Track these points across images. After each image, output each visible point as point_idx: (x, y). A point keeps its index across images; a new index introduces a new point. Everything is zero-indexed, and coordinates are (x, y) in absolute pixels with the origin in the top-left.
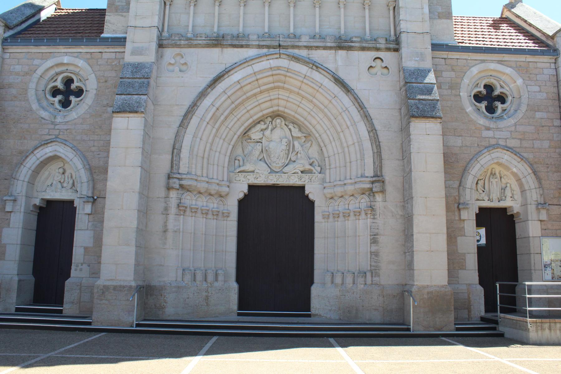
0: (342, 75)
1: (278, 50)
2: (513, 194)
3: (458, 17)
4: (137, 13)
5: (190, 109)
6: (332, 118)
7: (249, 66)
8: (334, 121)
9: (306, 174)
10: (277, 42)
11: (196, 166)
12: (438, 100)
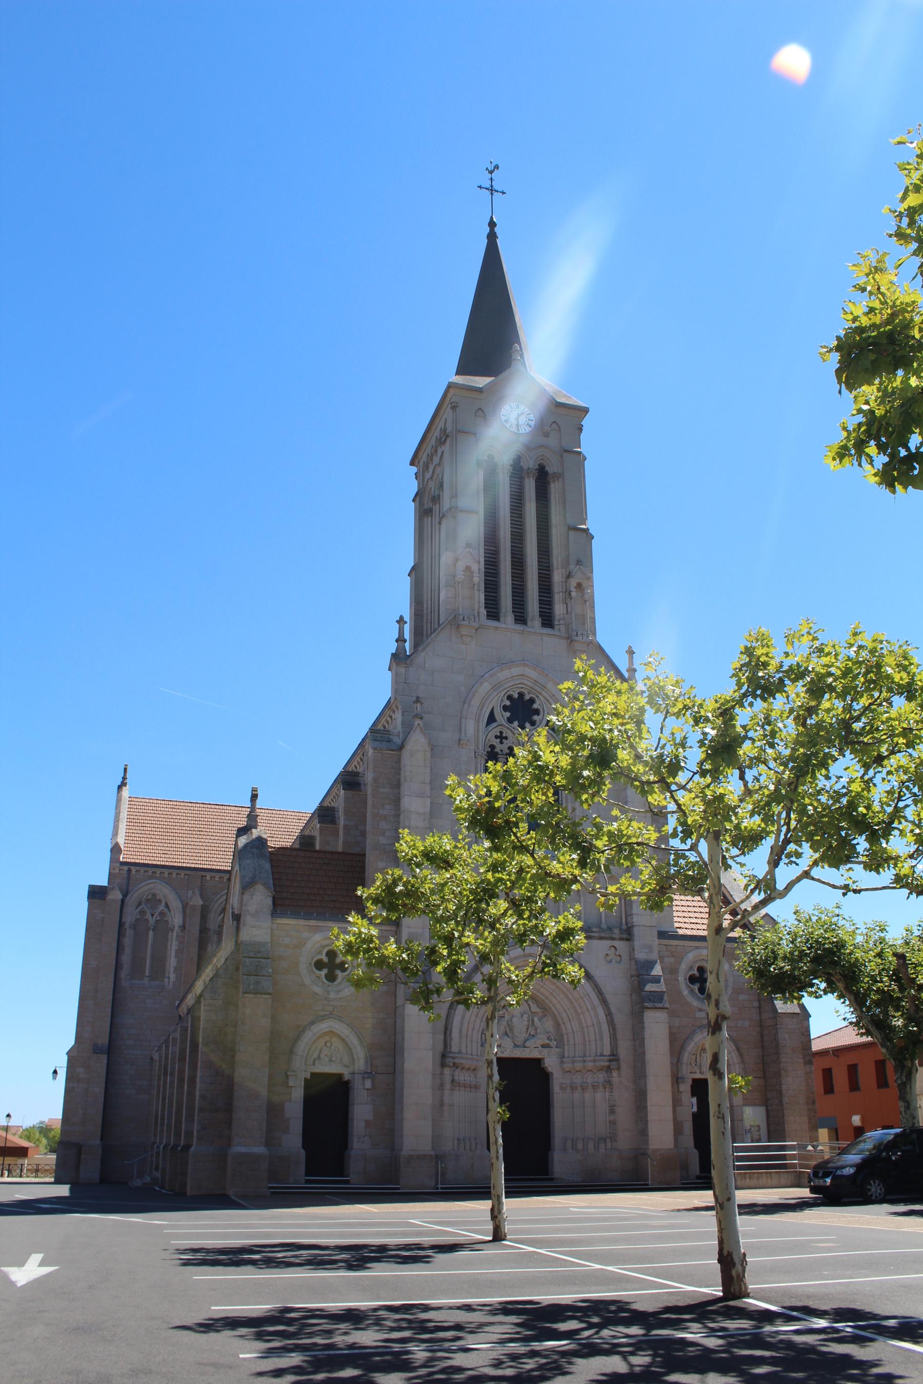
6: (574, 1001)
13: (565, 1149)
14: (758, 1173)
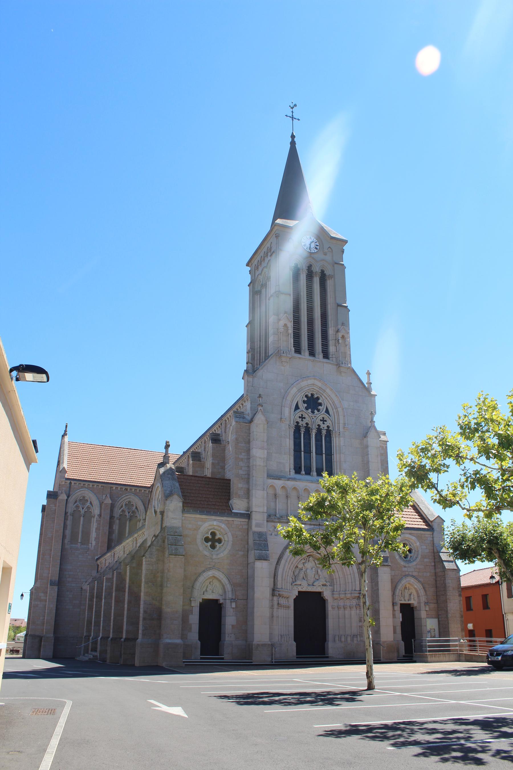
2: (414, 597)
13: (334, 641)
14: (439, 654)
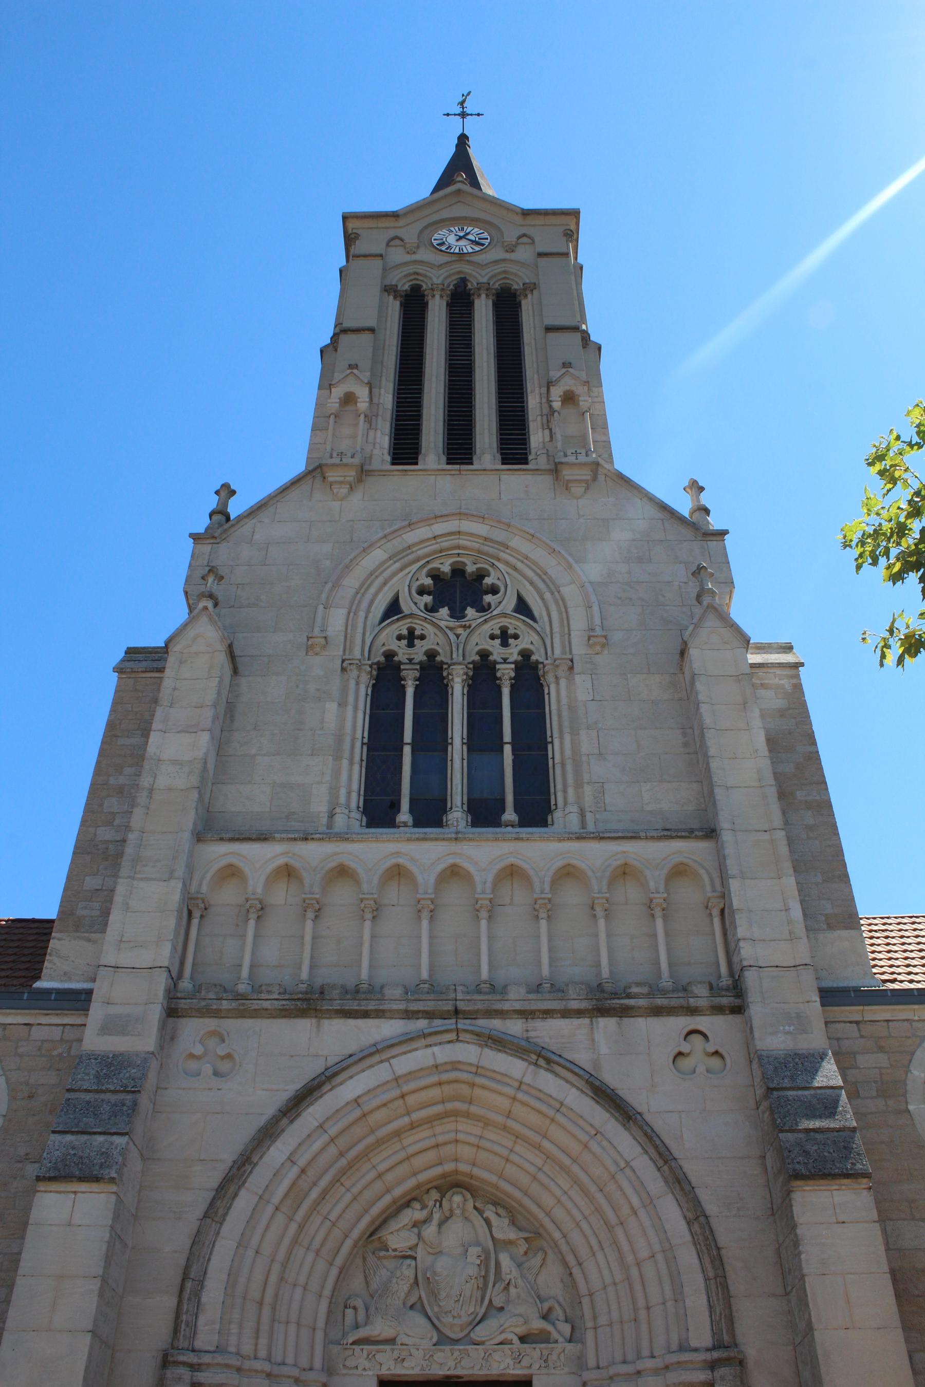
0: (610, 1077)
1: (455, 1020)
3: (874, 918)
4: (123, 936)
5: (235, 1170)
6: (593, 1188)
7: (382, 1062)
8: (599, 1196)
9: (534, 1345)
10: (451, 1002)
11: (241, 1327)
12: (854, 1130)
